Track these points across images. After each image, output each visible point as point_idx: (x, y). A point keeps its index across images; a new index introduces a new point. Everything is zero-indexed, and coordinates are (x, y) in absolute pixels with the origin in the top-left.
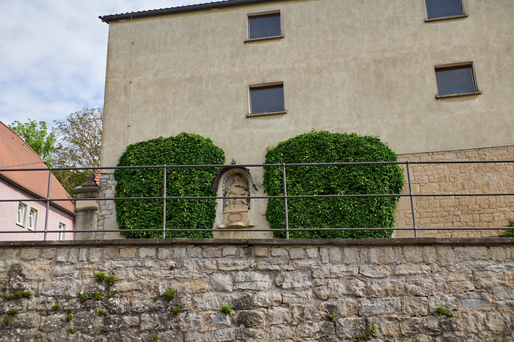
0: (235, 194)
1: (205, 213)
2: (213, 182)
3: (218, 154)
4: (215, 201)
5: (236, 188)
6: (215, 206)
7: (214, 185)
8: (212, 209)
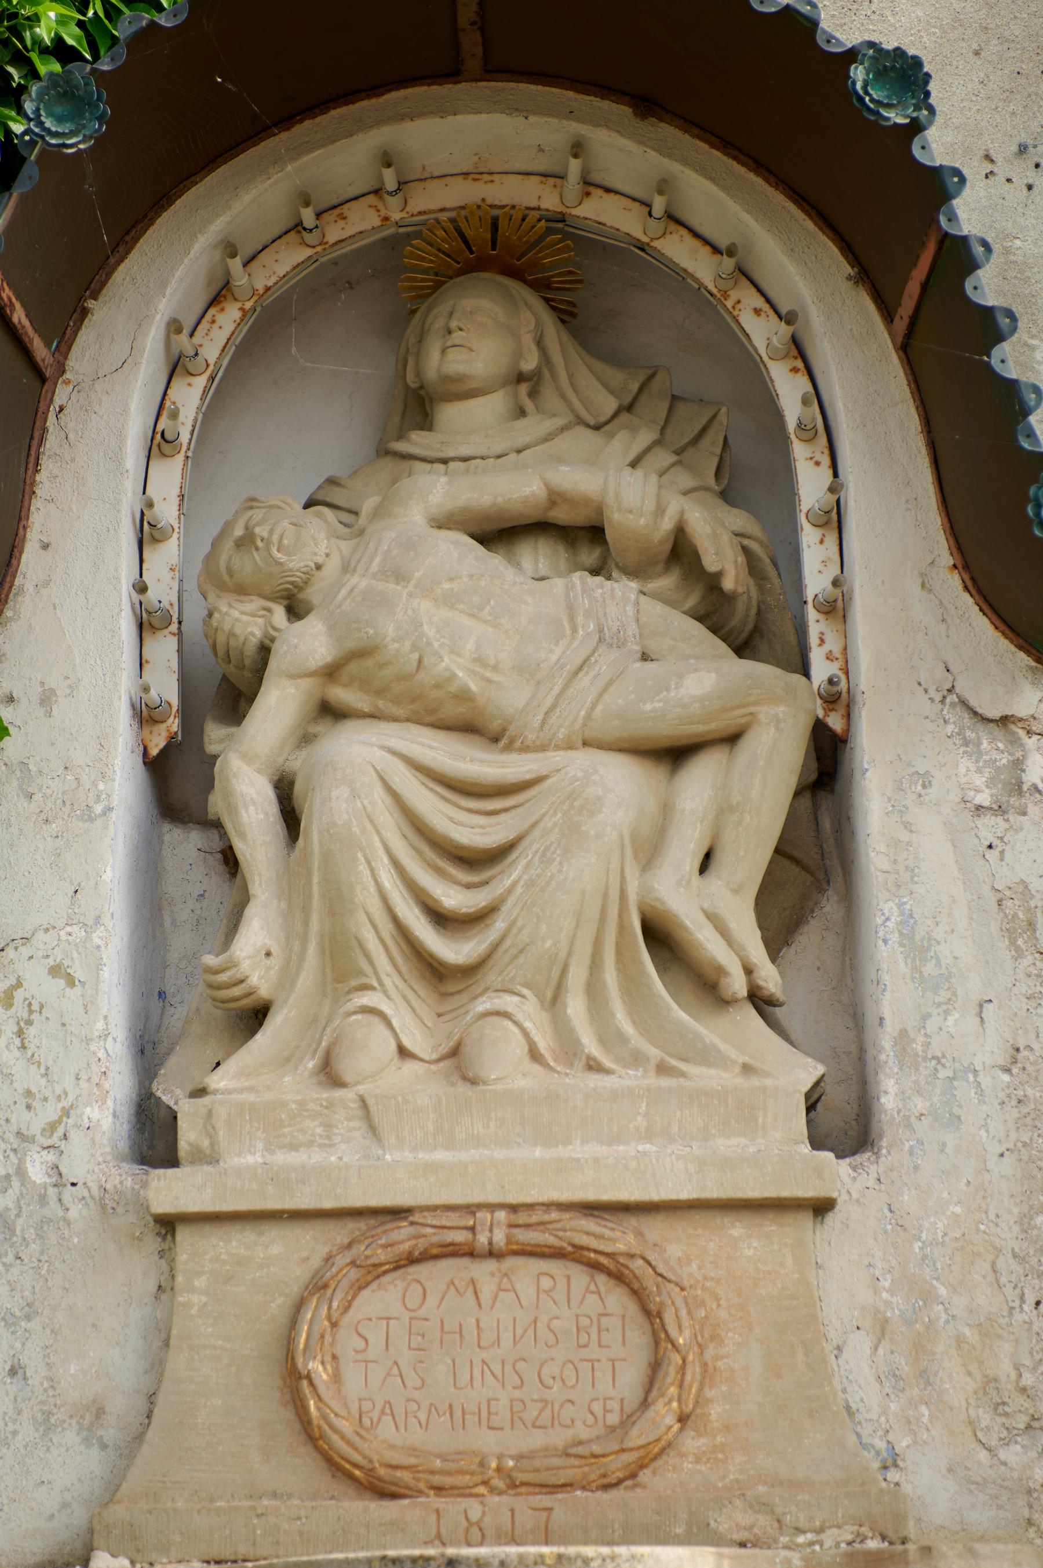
5: (493, 561)
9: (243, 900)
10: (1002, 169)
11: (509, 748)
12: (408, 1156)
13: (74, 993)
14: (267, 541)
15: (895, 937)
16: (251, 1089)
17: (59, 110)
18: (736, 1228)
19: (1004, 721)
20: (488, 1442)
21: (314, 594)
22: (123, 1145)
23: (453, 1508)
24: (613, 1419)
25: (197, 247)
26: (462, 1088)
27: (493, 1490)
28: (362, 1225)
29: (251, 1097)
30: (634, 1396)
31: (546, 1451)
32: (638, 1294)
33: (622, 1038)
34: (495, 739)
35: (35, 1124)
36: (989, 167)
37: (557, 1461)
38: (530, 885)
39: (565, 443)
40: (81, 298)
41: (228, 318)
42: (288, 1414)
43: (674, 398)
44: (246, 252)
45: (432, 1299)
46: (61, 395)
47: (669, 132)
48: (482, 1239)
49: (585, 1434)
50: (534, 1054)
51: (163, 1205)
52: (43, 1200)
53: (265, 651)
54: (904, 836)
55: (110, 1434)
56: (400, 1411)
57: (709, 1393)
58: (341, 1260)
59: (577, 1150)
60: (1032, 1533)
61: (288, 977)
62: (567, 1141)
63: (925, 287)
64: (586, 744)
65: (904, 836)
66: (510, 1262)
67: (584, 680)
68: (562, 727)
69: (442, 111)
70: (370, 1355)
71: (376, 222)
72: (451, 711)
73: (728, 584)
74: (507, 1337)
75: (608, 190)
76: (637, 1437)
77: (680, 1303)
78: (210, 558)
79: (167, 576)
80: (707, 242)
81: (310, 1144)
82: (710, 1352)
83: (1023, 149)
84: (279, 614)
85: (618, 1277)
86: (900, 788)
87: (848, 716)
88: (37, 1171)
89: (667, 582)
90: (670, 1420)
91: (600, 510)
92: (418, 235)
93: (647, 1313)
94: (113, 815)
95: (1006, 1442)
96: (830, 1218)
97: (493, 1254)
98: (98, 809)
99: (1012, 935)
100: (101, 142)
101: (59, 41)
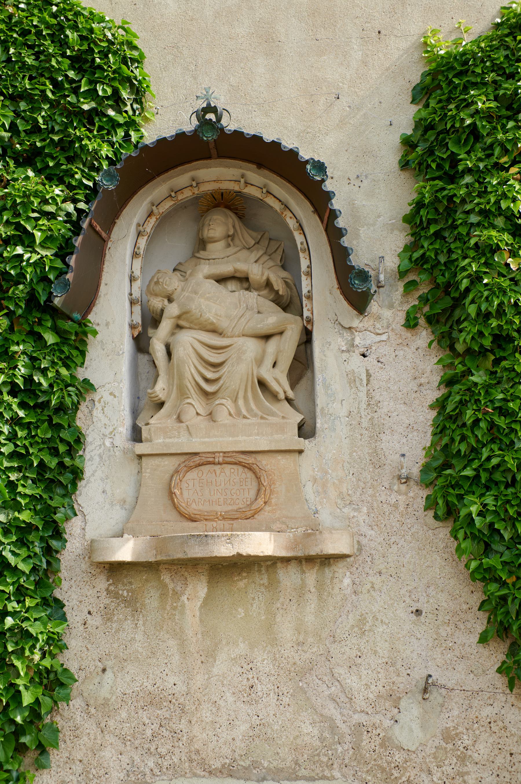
0: (214, 331)
1: (12, 456)
2: (68, 241)
3: (104, 55)
4: (81, 374)
5: (220, 288)
6: (76, 407)
7: (72, 261)
8: (59, 427)
9: (157, 376)
10: (352, 182)
11: (224, 337)
12: (198, 440)
13: (116, 399)
14: (162, 283)
15: (321, 384)
16: (160, 423)
17: (107, 179)
18: (279, 457)
19: (350, 328)
20: (218, 509)
21: (175, 296)
22: (129, 437)
23: (209, 524)
24: (248, 503)
25: (144, 204)
26: (212, 423)
27: (219, 520)
28: (187, 457)
29: (160, 425)
30: (253, 498)
31: (232, 510)
32: (255, 473)
33: (252, 410)
34: (221, 334)
35: (107, 432)
36: (349, 181)
37: (234, 513)
38: (229, 372)
39: (239, 254)
40: (114, 219)
41: (153, 220)
42: (170, 502)
43: (270, 239)
44: (156, 204)
45: (205, 475)
46: (110, 244)
47: (266, 172)
48: (217, 460)
49: (241, 506)
50: (230, 414)
51: (139, 452)
52: (109, 450)
53: (162, 311)
54: (324, 358)
55: (127, 507)
56: (197, 501)
57: (272, 497)
58: (182, 465)
59: (240, 438)
60: (349, 528)
61: (169, 395)
62: (238, 436)
63: (328, 218)
64: (243, 335)
65: (324, 358)
66: (224, 465)
67: (243, 319)
68: (237, 332)
69: (207, 167)
70: (190, 488)
71: (191, 194)
72: (209, 327)
73: (281, 293)
74: (223, 484)
75: (252, 185)
76: (254, 507)
77: (265, 475)
78: (148, 286)
79: (138, 290)
80: (278, 199)
81: (174, 437)
82: (272, 487)
83: (358, 177)
84: (166, 301)
85: (250, 469)
86: (323, 346)
87: (313, 325)
88: (108, 443)
89: (265, 292)
90: (262, 503)
91: (247, 274)
92: (202, 197)
93: (257, 478)
94: (125, 354)
95: (344, 507)
96: (303, 454)
97: (219, 463)
98: (121, 352)
99: (350, 383)
100: (117, 187)
101: (107, 156)
